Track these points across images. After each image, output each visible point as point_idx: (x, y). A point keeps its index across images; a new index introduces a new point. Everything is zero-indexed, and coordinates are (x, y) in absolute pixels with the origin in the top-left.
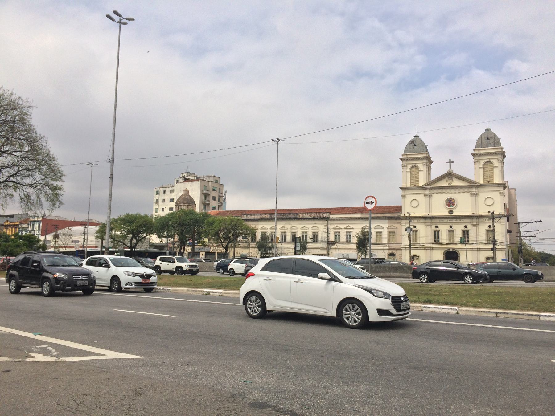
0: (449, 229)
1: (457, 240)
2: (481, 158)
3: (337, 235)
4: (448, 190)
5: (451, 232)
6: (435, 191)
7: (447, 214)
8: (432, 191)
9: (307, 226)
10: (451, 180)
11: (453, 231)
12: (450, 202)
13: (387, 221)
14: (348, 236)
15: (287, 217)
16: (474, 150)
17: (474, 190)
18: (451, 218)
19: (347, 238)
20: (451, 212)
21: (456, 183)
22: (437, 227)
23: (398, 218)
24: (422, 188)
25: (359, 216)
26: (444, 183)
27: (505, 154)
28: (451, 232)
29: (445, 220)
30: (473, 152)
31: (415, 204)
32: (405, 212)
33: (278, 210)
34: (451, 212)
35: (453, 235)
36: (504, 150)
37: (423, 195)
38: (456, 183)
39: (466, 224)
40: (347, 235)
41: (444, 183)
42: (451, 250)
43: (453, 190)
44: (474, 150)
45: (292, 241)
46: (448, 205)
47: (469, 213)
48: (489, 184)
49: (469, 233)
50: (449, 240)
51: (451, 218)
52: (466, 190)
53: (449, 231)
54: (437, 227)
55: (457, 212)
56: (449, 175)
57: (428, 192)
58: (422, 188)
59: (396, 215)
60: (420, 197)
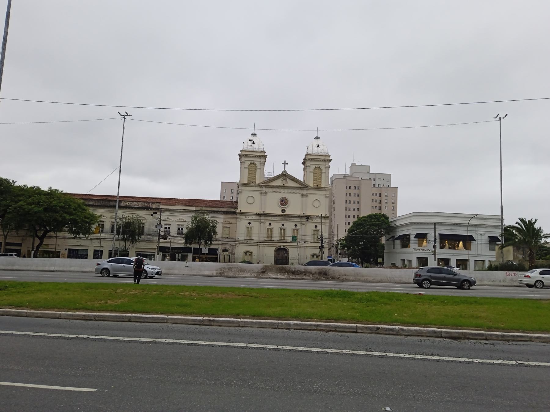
0: (294, 227)
1: (289, 238)
2: (247, 159)
3: (168, 229)
4: (282, 190)
5: (283, 230)
6: (271, 190)
7: (280, 212)
8: (267, 190)
9: (104, 214)
11: (251, 228)
12: (284, 202)
13: (223, 216)
14: (180, 230)
15: (108, 204)
16: (241, 151)
17: (305, 192)
18: (283, 216)
19: (178, 232)
20: (283, 211)
21: (290, 183)
22: (270, 224)
23: (234, 213)
24: (259, 186)
25: (194, 208)
26: (278, 183)
27: (303, 161)
28: (283, 230)
29: (278, 219)
30: (240, 153)
31: (250, 200)
32: (242, 207)
33: (120, 197)
34: (283, 211)
35: (284, 232)
36: (266, 154)
37: (258, 193)
38: (290, 183)
39: (270, 222)
40: (179, 229)
41: (278, 183)
42: (282, 247)
43: (286, 190)
44: (241, 151)
45: (112, 232)
46: (281, 204)
47: (298, 213)
48: (317, 187)
49: (273, 230)
50: (247, 236)
51: (283, 216)
52: (298, 191)
53: (281, 229)
54: (270, 224)
56: (284, 176)
57: (264, 189)
58: (259, 186)
59: (233, 210)
60: (255, 193)
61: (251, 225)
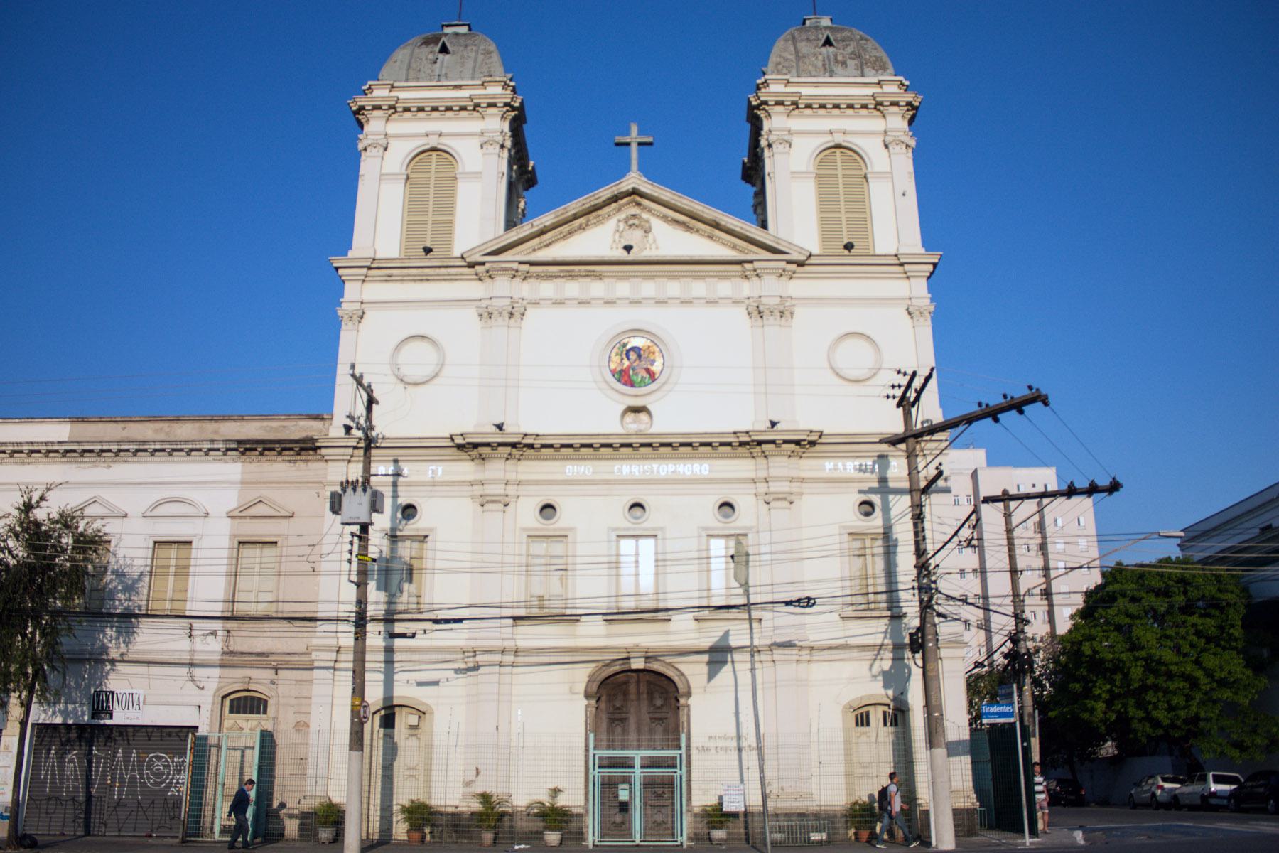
6: (547, 289)
8: (525, 289)
10: (638, 233)
17: (770, 288)
52: (725, 288)
55: (671, 414)
57: (503, 288)
59: (297, 429)
61: (562, 520)
